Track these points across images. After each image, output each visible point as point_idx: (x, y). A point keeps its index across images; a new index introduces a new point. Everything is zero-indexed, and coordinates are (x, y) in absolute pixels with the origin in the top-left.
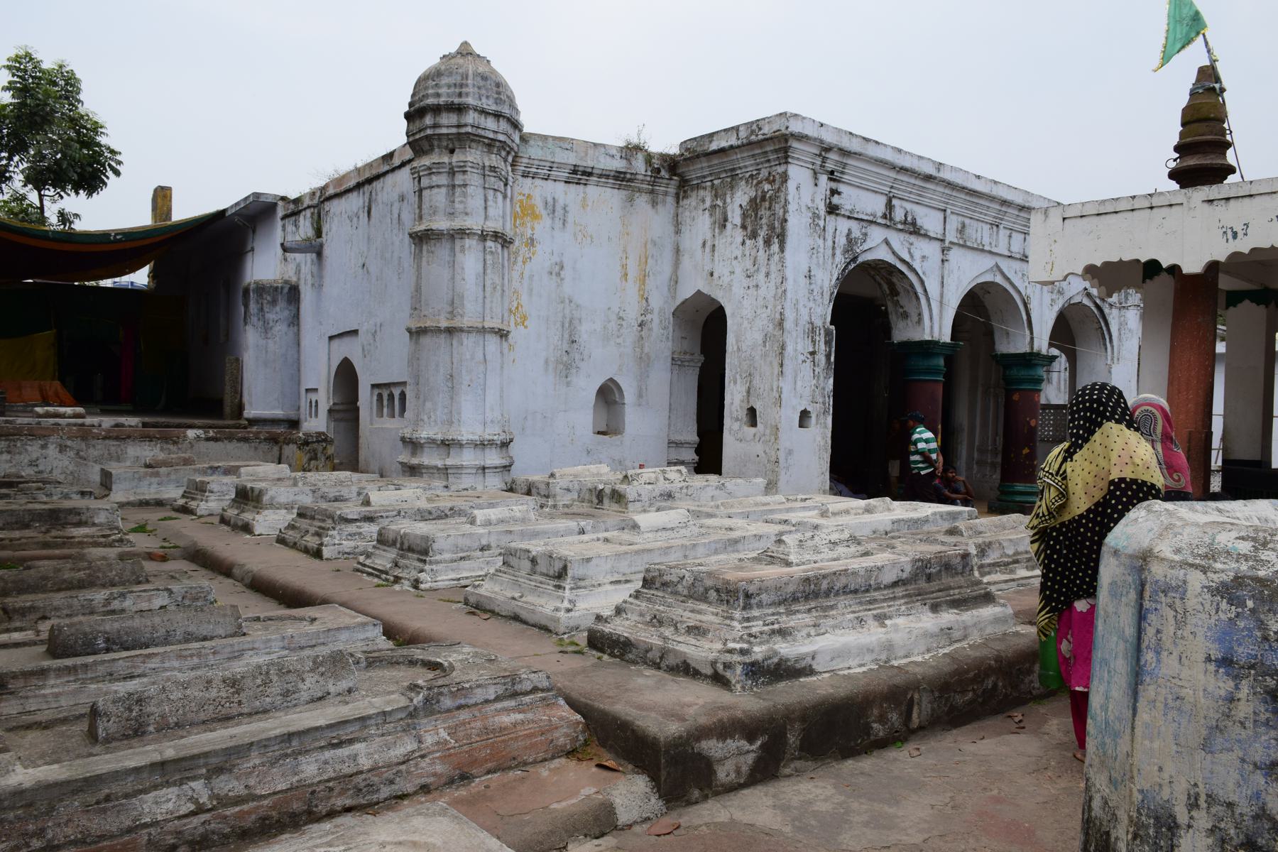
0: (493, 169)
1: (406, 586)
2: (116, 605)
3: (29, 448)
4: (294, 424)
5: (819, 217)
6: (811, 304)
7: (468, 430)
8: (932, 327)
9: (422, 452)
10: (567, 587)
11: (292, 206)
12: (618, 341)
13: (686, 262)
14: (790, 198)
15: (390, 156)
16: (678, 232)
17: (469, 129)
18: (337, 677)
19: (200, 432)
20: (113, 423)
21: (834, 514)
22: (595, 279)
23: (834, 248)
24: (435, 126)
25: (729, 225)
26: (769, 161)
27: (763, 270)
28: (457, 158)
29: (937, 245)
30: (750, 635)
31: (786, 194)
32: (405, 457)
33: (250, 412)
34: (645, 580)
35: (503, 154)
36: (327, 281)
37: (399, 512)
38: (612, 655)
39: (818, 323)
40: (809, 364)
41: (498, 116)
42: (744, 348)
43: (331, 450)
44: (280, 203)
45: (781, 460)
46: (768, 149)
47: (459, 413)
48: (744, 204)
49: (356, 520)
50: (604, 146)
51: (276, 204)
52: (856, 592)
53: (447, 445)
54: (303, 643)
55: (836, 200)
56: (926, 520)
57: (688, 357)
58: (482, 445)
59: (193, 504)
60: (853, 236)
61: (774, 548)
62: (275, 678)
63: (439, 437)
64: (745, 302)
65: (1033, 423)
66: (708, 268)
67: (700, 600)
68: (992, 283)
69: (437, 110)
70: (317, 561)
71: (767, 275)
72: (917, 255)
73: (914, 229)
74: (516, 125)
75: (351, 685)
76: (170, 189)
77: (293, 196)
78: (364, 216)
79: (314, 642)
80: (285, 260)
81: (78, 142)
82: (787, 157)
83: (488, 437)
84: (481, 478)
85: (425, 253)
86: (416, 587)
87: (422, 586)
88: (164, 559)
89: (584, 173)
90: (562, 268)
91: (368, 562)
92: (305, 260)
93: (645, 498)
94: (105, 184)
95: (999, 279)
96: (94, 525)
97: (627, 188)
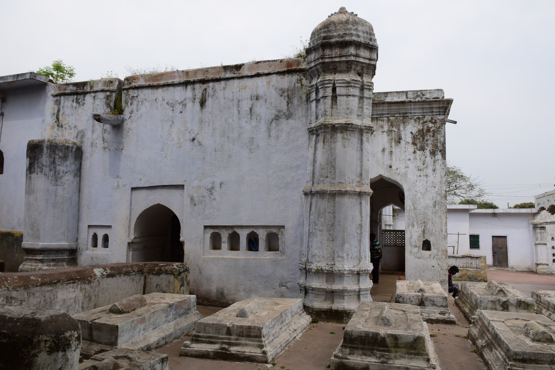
4: (72, 254)
15: (238, 67)
25: (402, 142)
26: (432, 112)
42: (419, 208)
46: (434, 106)
48: (414, 132)
66: (388, 163)
71: (434, 170)
82: (445, 112)
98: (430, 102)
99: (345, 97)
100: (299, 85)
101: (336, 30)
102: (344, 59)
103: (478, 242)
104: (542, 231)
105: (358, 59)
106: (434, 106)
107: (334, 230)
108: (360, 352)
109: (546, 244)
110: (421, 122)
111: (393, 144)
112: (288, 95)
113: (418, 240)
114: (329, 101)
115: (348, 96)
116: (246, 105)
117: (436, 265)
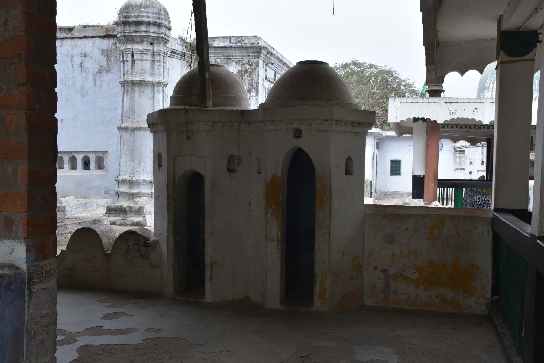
17: (163, 35)
24: (147, 32)
26: (249, 56)
28: (156, 48)
82: (259, 56)
98: (246, 48)
99: (140, 62)
100: (115, 47)
101: (133, 12)
102: (138, 34)
103: (400, 168)
104: (462, 155)
105: (148, 34)
106: (250, 51)
107: (133, 154)
108: (113, 215)
109: (464, 169)
110: (241, 64)
112: (107, 54)
114: (129, 64)
115: (142, 60)
116: (77, 60)
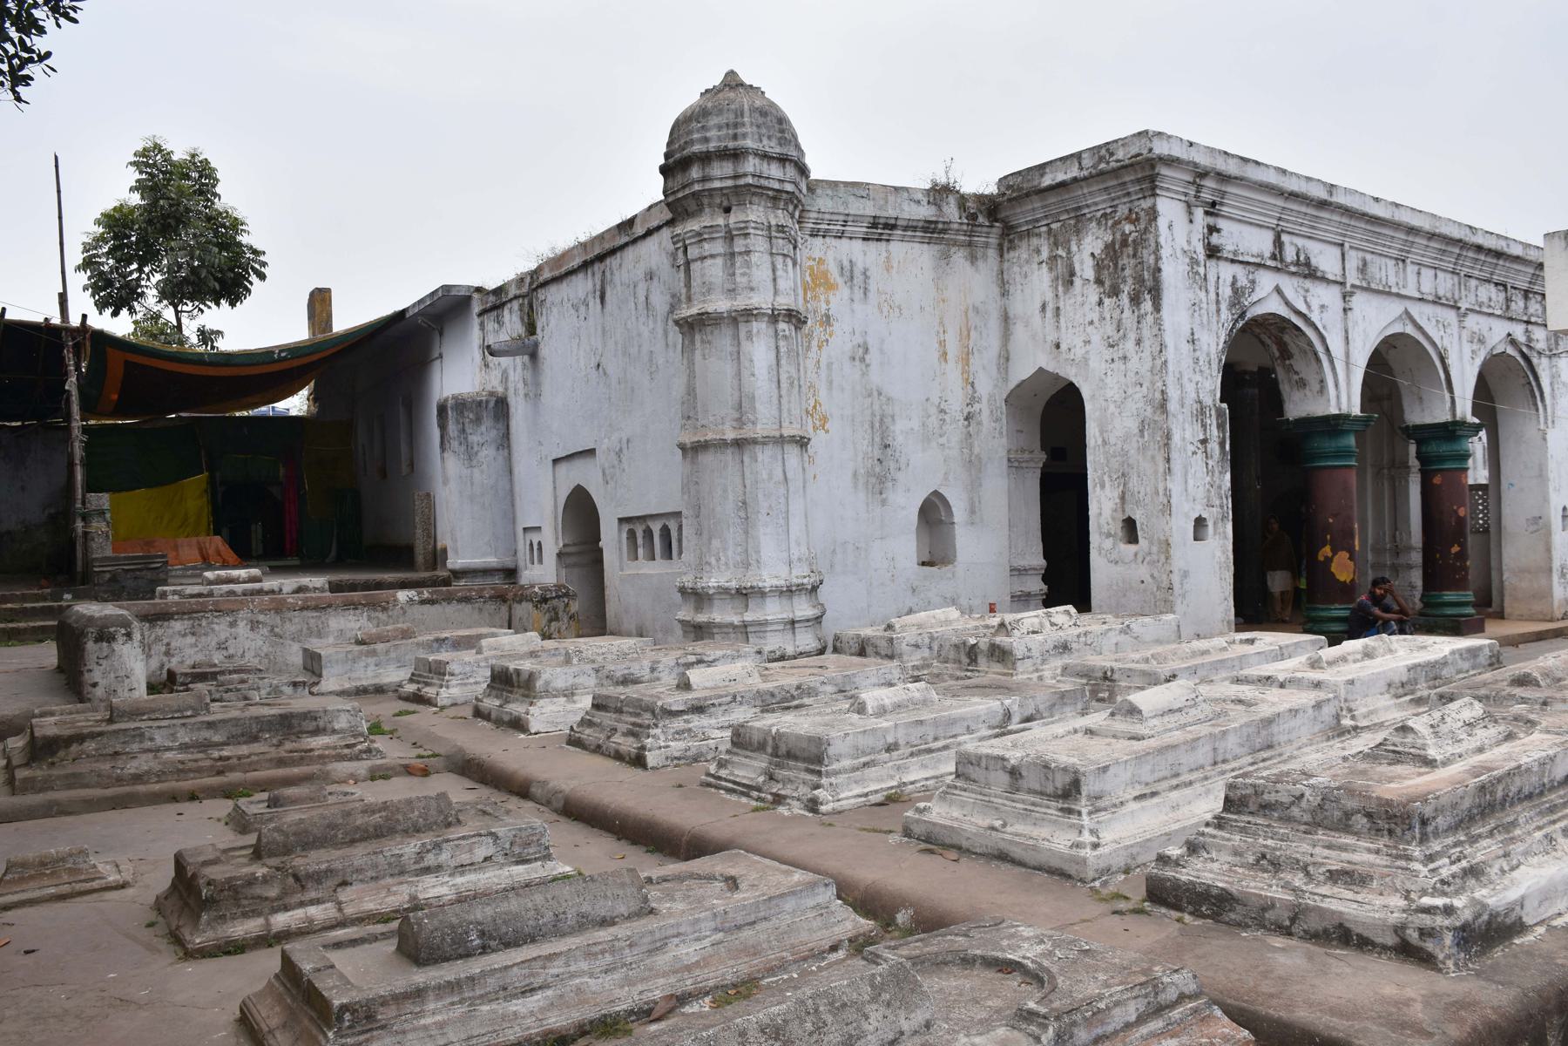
0: (781, 228)
1: (798, 809)
2: (430, 859)
3: (216, 627)
4: (511, 573)
5: (1198, 264)
6: (1198, 377)
7: (771, 575)
8: (1338, 397)
9: (711, 606)
10: (1084, 811)
11: (492, 298)
12: (942, 440)
13: (1020, 333)
14: (1162, 240)
15: (629, 224)
16: (1005, 293)
17: (750, 180)
18: (909, 1008)
19: (412, 593)
20: (295, 586)
21: (1330, 663)
22: (911, 362)
23: (1218, 302)
24: (705, 179)
25: (1078, 282)
26: (1128, 194)
27: (1132, 336)
28: (734, 218)
29: (1336, 290)
30: (1443, 882)
31: (1157, 236)
32: (686, 613)
33: (455, 561)
34: (1227, 799)
35: (791, 208)
36: (546, 389)
37: (735, 697)
38: (1196, 914)
39: (1208, 401)
40: (1200, 456)
41: (783, 160)
42: (1112, 440)
43: (575, 607)
44: (476, 296)
45: (1176, 586)
46: (1127, 179)
47: (758, 552)
48: (1097, 252)
49: (681, 712)
50: (906, 189)
51: (469, 298)
52: (1530, 797)
53: (744, 595)
54: (740, 920)
55: (1215, 239)
56: (1444, 663)
57: (1026, 456)
58: (789, 592)
59: (429, 691)
60: (1239, 284)
61: (1397, 740)
62: (829, 1019)
63: (734, 584)
64: (1108, 380)
65: (1462, 512)
67: (1337, 830)
68: (1402, 334)
69: (706, 158)
70: (640, 771)
71: (1139, 342)
72: (1315, 304)
73: (1308, 272)
74: (803, 170)
75: (928, 1016)
76: (329, 290)
77: (491, 285)
78: (595, 304)
79: (752, 918)
80: (487, 366)
81: (217, 245)
82: (1154, 188)
83: (795, 581)
84: (789, 636)
85: (698, 344)
86: (814, 811)
87: (823, 808)
88: (425, 773)
89: (887, 226)
90: (866, 350)
91: (723, 773)
92: (515, 366)
93: (1035, 653)
94: (249, 291)
95: (1410, 330)
96: (334, 731)
97: (939, 241)
102: (687, 191)
105: (709, 185)
110: (1110, 222)
111: (1060, 289)
113: (1114, 519)
115: (703, 258)
117: (1148, 579)
